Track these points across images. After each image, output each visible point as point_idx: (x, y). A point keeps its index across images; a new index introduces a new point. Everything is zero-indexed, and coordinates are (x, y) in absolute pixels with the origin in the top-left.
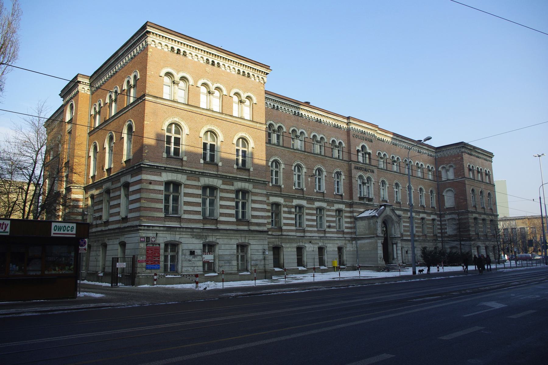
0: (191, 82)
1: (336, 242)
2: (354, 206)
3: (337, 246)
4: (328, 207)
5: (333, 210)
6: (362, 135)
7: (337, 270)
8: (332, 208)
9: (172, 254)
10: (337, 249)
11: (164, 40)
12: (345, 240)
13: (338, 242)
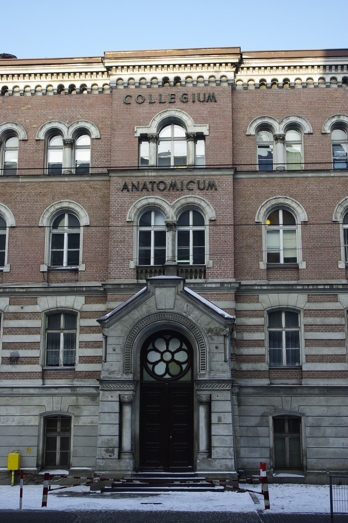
0: (307, 128)
1: (36, 401)
2: (110, 296)
3: (37, 412)
4: (13, 309)
5: (34, 315)
6: (167, 90)
7: (16, 483)
8: (29, 309)
9: (51, 435)
10: (35, 421)
11: (205, 69)
12: (77, 395)
13: (45, 401)
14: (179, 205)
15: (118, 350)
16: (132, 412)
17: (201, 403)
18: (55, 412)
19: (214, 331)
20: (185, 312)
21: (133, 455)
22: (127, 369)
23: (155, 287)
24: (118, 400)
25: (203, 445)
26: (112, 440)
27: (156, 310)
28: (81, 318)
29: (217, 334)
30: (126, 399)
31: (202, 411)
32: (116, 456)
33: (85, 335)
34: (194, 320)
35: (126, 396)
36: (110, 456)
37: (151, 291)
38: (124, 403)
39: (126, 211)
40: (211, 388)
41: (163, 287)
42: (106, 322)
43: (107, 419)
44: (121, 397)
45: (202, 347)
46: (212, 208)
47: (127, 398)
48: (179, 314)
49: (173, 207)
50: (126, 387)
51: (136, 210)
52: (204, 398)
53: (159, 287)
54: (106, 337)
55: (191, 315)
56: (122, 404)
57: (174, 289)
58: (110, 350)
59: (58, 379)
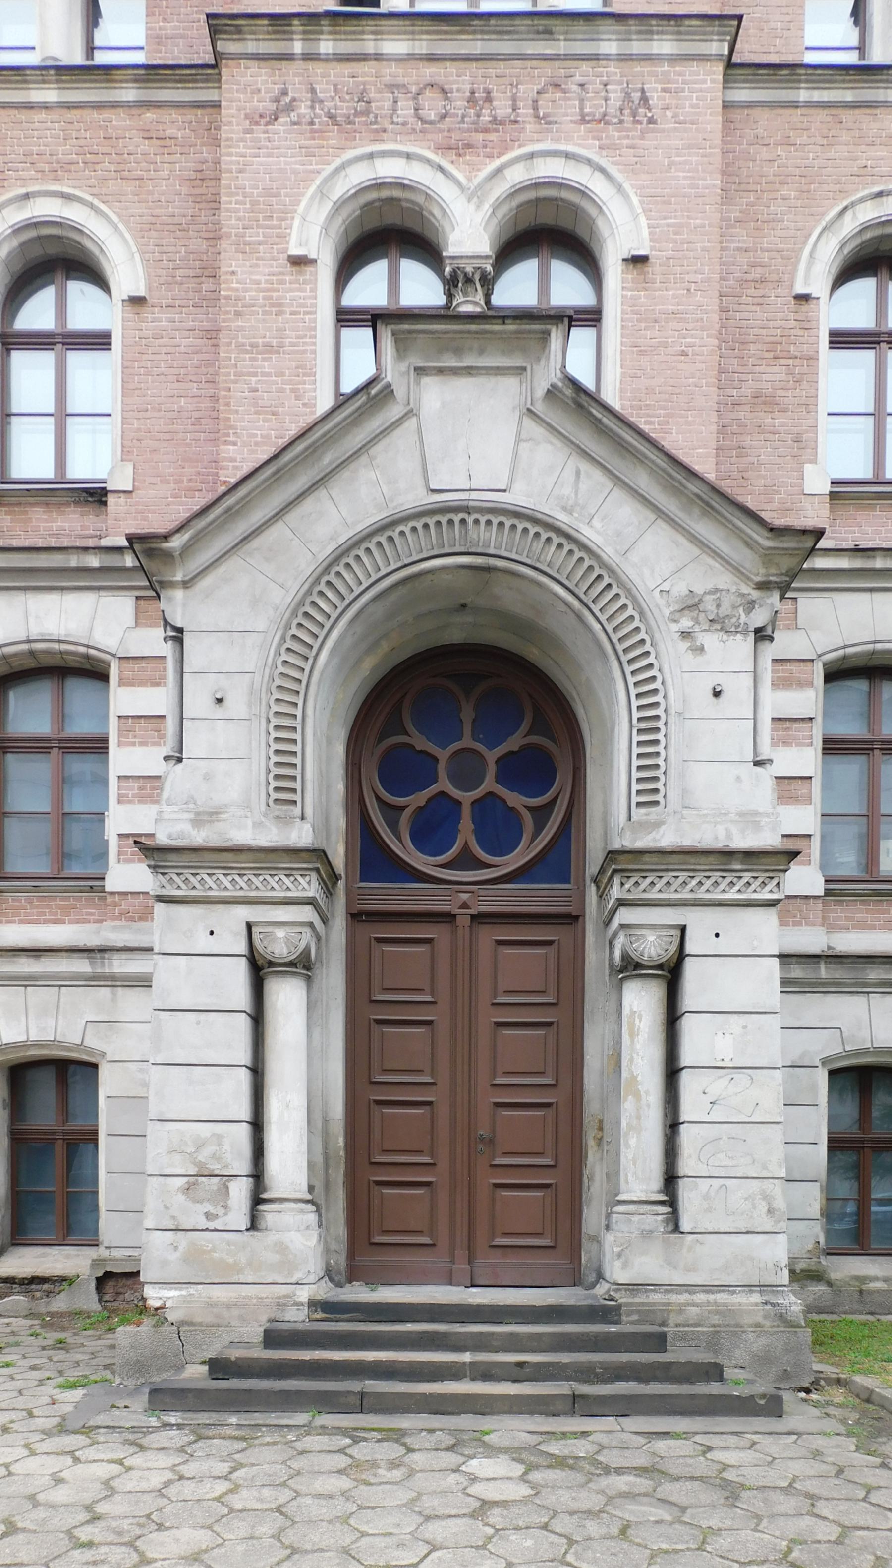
14: (501, 189)
15: (237, 705)
16: (309, 1018)
17: (631, 967)
18: (38, 1045)
19: (709, 604)
20: (564, 509)
21: (318, 1211)
22: (284, 790)
23: (420, 371)
24: (241, 947)
25: (640, 1176)
26: (219, 1138)
27: (421, 491)
28: (122, 683)
29: (719, 624)
30: (279, 945)
31: (642, 1001)
32: (239, 1217)
33: (139, 751)
34: (609, 550)
35: (280, 933)
36: (208, 1216)
37: (400, 392)
38: (271, 964)
39: (286, 214)
40: (685, 895)
41: (455, 372)
42: (176, 543)
43: (189, 1037)
44: (256, 937)
45: (648, 692)
46: (635, 200)
47: (287, 940)
48: (536, 521)
49: (475, 195)
50: (279, 885)
51: (328, 206)
52: (653, 948)
53: (441, 371)
54: (178, 636)
55: (596, 523)
56: (260, 970)
57: (511, 383)
58: (197, 701)
59: (46, 922)
